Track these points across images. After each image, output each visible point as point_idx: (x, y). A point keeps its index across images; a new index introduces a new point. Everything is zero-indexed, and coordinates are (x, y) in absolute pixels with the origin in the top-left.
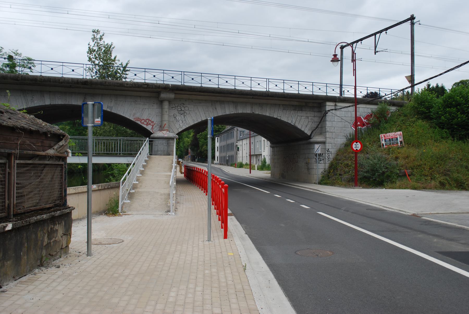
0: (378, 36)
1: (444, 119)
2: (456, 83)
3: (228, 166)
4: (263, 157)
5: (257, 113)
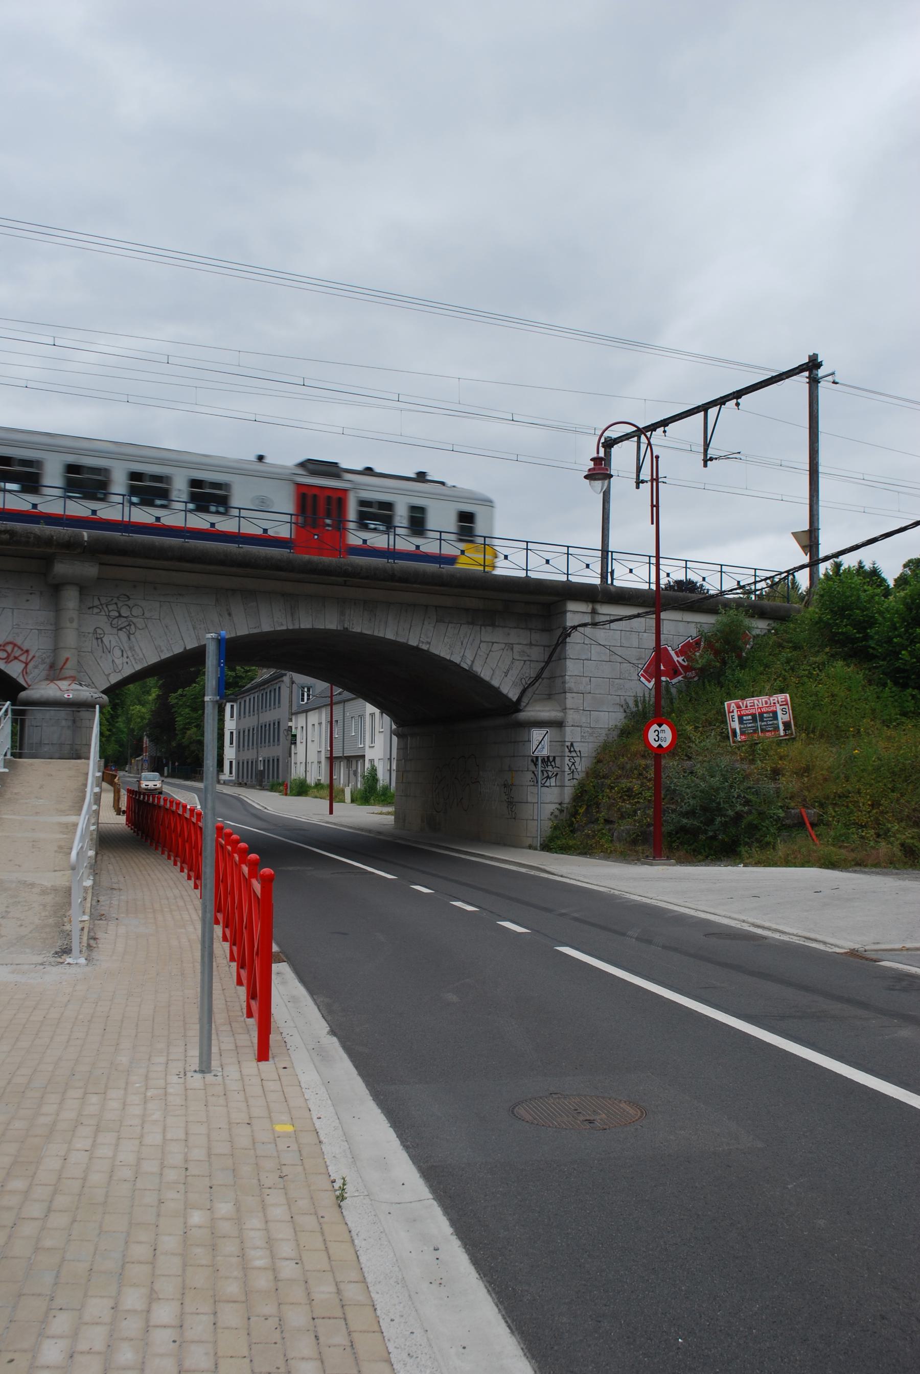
0: (712, 412)
1: (907, 658)
2: (910, 561)
3: (263, 788)
4: (367, 765)
5: (357, 629)
